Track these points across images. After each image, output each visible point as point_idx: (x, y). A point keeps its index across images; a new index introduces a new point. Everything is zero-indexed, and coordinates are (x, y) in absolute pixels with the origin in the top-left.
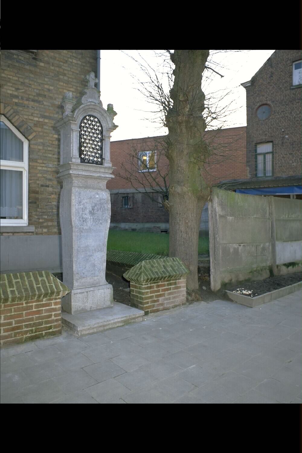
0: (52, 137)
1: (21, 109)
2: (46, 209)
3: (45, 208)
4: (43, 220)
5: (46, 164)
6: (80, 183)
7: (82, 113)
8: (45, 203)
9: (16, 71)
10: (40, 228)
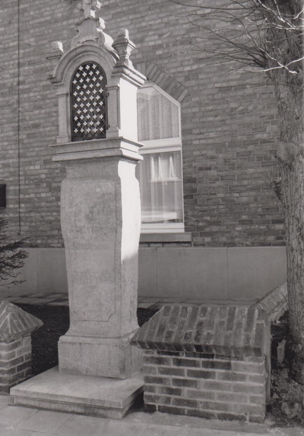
0: (212, 88)
1: (166, 61)
2: (207, 205)
3: (206, 204)
4: (204, 224)
5: (205, 134)
6: (76, 173)
7: (68, 66)
8: (207, 196)
9: (158, 11)
10: (201, 236)
